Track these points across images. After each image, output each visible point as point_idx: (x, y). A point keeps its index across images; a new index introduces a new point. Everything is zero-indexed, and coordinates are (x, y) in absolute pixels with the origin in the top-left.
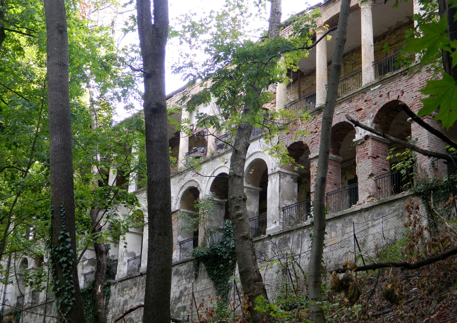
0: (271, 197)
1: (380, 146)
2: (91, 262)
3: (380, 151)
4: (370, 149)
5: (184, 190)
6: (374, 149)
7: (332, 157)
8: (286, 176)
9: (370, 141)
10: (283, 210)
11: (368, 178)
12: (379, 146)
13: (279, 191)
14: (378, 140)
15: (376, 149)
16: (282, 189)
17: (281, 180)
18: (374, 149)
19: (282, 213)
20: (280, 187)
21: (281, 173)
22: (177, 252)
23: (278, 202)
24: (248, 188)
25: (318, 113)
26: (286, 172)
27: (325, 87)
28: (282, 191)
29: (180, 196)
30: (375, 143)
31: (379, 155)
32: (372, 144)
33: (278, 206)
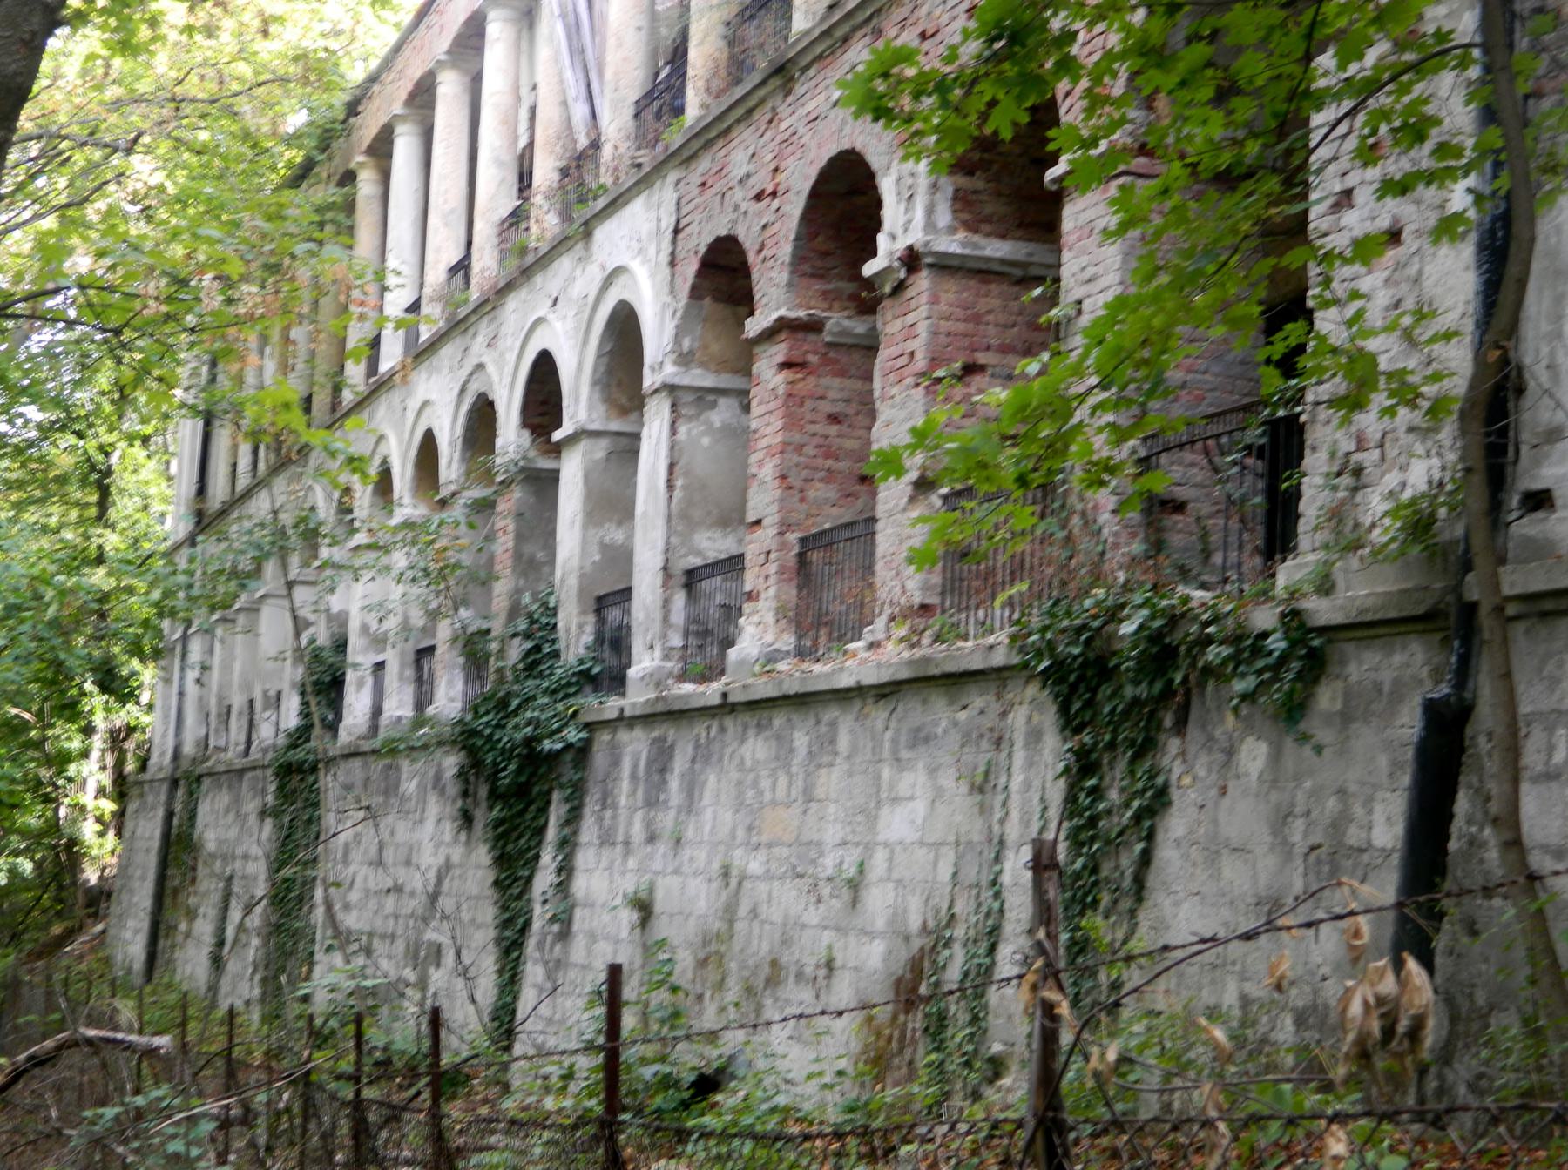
0: (645, 513)
1: (995, 303)
2: (89, 161)
3: (991, 330)
4: (923, 329)
5: (465, 408)
6: (945, 326)
7: (845, 332)
8: (713, 405)
9: (923, 282)
10: (691, 579)
11: (912, 499)
12: (983, 305)
13: (670, 486)
14: (980, 271)
15: (961, 327)
16: (686, 474)
17: (682, 429)
18: (945, 326)
19: (680, 599)
20: (671, 467)
21: (679, 393)
22: (450, 683)
23: (660, 545)
24: (618, 434)
25: (783, 86)
26: (707, 380)
27: (722, 30)
28: (684, 487)
29: (459, 430)
30: (953, 291)
31: (982, 358)
32: (934, 301)
33: (660, 564)
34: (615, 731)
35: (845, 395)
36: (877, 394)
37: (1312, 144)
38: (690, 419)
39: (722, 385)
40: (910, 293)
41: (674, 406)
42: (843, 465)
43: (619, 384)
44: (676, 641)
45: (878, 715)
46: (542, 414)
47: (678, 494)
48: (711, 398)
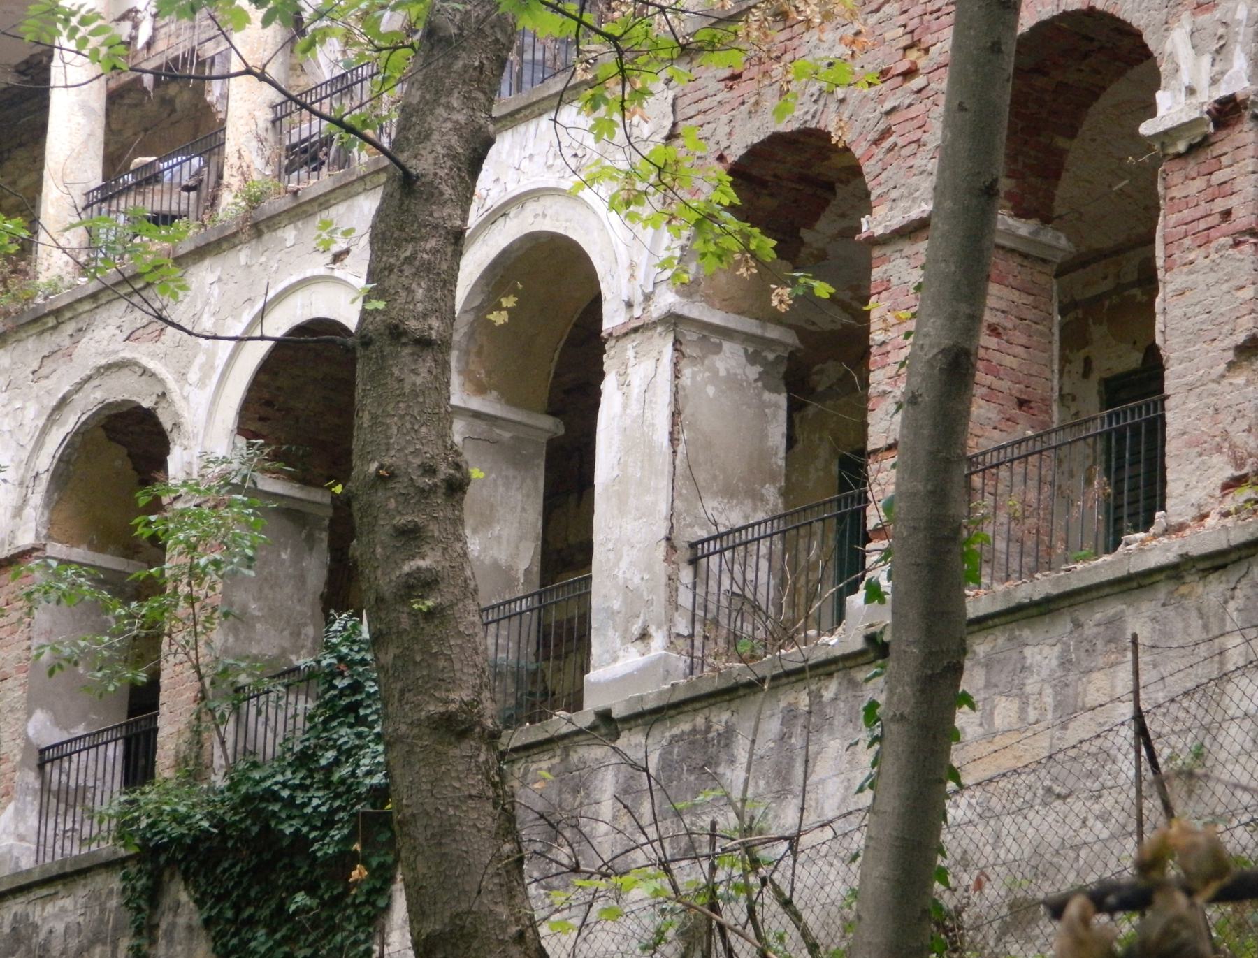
8: (718, 349)
11: (1231, 366)
13: (673, 440)
17: (687, 372)
19: (686, 575)
21: (682, 328)
23: (663, 508)
26: (717, 318)
33: (663, 532)
34: (566, 751)
35: (1003, 305)
36: (1159, 262)
37: (271, 343)
38: (694, 360)
39: (732, 325)
40: (1217, 150)
41: (677, 343)
42: (1004, 385)
43: (479, 353)
44: (682, 627)
45: (1212, 590)
46: (262, 419)
47: (681, 448)
48: (714, 340)
